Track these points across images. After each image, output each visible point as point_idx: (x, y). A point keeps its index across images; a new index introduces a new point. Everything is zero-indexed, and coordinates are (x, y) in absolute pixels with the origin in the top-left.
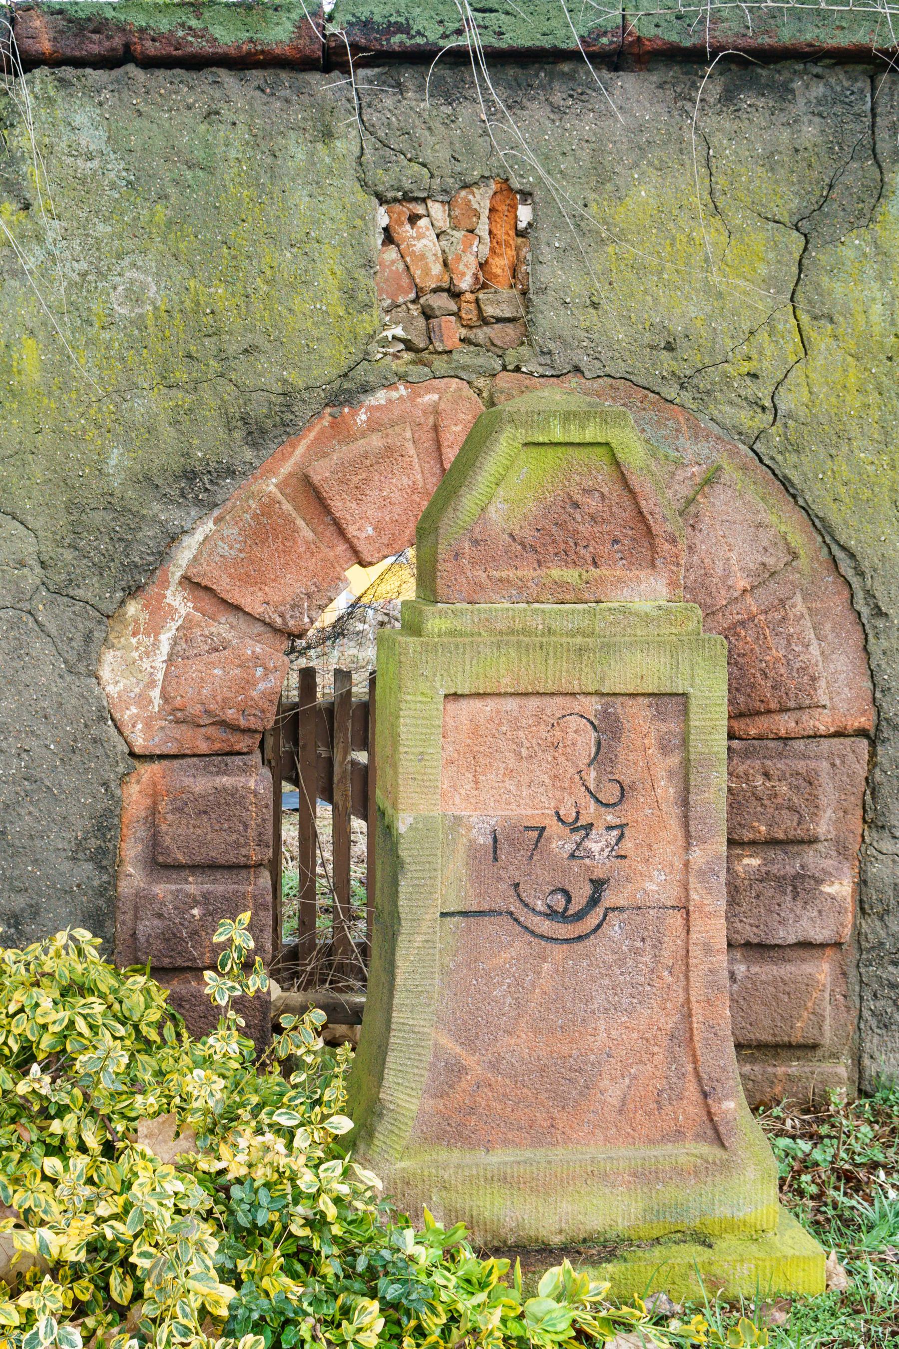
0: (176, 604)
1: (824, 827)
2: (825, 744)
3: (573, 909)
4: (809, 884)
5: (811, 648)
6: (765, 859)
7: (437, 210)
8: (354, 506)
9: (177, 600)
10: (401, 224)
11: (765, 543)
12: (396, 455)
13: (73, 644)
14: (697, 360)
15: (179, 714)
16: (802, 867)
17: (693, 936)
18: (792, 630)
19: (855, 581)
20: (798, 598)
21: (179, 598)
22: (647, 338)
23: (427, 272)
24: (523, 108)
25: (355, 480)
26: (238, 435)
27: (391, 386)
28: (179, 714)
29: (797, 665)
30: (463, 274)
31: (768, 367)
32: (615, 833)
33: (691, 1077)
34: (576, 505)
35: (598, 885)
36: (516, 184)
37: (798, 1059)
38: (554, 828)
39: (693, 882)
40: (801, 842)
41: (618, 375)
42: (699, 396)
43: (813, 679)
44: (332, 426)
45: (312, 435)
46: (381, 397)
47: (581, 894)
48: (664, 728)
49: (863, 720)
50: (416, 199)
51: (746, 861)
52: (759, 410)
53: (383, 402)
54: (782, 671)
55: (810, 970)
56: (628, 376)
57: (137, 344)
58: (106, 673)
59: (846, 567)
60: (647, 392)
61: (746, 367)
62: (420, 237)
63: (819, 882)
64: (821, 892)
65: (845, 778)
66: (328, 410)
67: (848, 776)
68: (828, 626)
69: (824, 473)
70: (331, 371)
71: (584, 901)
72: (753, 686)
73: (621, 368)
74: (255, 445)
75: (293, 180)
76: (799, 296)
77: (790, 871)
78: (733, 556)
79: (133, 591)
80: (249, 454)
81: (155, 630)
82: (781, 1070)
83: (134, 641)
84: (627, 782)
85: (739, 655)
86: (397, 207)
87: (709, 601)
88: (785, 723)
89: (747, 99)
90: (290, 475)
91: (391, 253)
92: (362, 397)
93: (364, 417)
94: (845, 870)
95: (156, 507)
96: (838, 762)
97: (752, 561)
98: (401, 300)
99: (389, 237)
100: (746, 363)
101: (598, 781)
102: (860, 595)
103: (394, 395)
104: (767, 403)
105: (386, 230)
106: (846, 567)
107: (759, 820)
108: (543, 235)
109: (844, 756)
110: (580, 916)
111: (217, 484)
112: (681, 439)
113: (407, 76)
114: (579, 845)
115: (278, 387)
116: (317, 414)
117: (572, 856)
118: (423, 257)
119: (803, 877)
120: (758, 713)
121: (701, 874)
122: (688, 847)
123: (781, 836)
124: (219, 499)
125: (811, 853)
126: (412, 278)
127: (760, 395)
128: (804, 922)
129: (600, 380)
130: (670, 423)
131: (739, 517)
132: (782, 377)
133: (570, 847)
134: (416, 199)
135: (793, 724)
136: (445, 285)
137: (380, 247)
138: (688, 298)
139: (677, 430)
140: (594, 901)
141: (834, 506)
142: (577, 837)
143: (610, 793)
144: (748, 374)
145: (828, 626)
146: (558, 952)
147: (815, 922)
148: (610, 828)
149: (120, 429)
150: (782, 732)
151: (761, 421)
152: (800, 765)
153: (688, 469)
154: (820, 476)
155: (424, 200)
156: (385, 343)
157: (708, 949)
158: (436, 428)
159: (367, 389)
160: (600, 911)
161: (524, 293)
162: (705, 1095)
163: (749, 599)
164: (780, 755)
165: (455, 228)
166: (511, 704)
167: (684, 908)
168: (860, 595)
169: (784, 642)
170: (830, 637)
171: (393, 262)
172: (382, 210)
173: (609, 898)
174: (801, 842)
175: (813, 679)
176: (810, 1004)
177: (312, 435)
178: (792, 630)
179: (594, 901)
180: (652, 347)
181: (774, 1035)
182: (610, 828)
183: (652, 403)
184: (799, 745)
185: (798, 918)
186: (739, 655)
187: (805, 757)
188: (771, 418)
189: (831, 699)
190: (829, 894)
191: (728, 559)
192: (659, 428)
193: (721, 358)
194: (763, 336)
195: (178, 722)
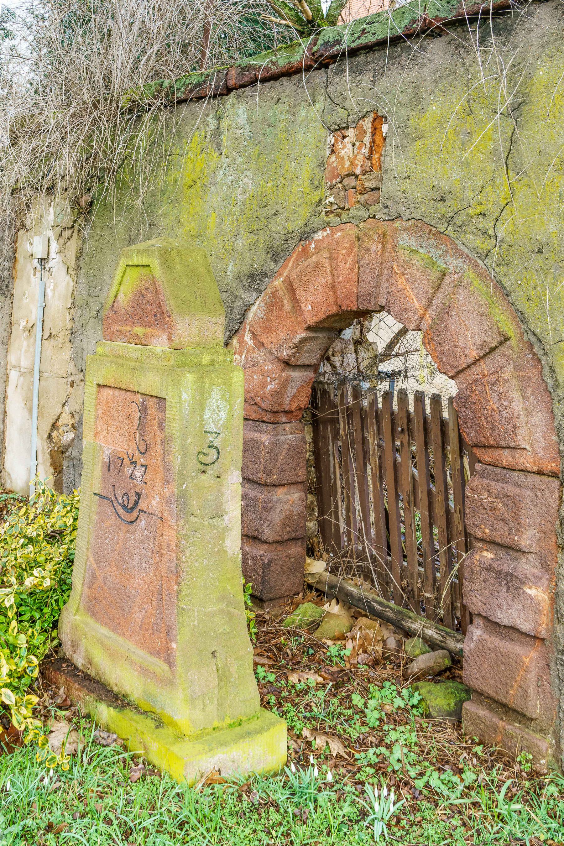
1: (527, 539)
2: (531, 479)
4: (516, 583)
5: (514, 404)
6: (496, 556)
8: (303, 293)
11: (486, 327)
12: (320, 266)
14: (455, 206)
18: (502, 390)
20: (511, 367)
22: (432, 194)
25: (305, 279)
26: (269, 256)
27: (324, 229)
29: (505, 415)
30: (357, 165)
31: (492, 210)
32: (143, 469)
34: (143, 295)
37: (520, 723)
41: (417, 218)
42: (457, 229)
43: (515, 427)
45: (295, 255)
46: (319, 235)
49: (553, 464)
51: (485, 553)
52: (488, 237)
53: (321, 237)
54: (496, 418)
55: (519, 652)
56: (422, 218)
57: (242, 213)
60: (431, 227)
61: (478, 210)
63: (523, 583)
64: (524, 592)
65: (543, 508)
67: (546, 506)
68: (530, 390)
69: (521, 280)
70: (300, 222)
72: (479, 425)
73: (417, 214)
74: (275, 261)
75: (299, 126)
76: (509, 161)
77: (505, 568)
78: (469, 334)
80: (272, 265)
82: (501, 724)
85: (471, 402)
87: (455, 364)
88: (506, 457)
92: (313, 235)
93: (313, 246)
94: (544, 580)
95: (241, 291)
96: (539, 494)
97: (479, 338)
100: (479, 207)
103: (325, 233)
104: (491, 233)
106: (537, 348)
107: (484, 524)
109: (543, 490)
111: (262, 280)
112: (448, 257)
115: (283, 232)
119: (512, 575)
120: (491, 447)
124: (262, 288)
125: (525, 560)
127: (487, 227)
128: (512, 611)
129: (410, 222)
130: (443, 247)
131: (471, 308)
132: (498, 215)
135: (511, 459)
138: (451, 168)
139: (446, 251)
140: (136, 503)
141: (527, 304)
144: (481, 214)
145: (530, 390)
147: (520, 614)
149: (233, 254)
151: (488, 245)
152: (510, 489)
153: (452, 276)
154: (519, 282)
159: (315, 231)
164: (503, 480)
166: (117, 393)
169: (497, 398)
170: (532, 398)
173: (142, 505)
175: (515, 427)
176: (518, 679)
177: (295, 255)
178: (502, 390)
180: (435, 200)
181: (497, 694)
183: (434, 235)
184: (515, 475)
185: (509, 607)
186: (471, 402)
187: (517, 485)
188: (494, 242)
189: (532, 445)
190: (528, 594)
191: (466, 337)
192: (437, 250)
193: (466, 204)
194: (488, 189)
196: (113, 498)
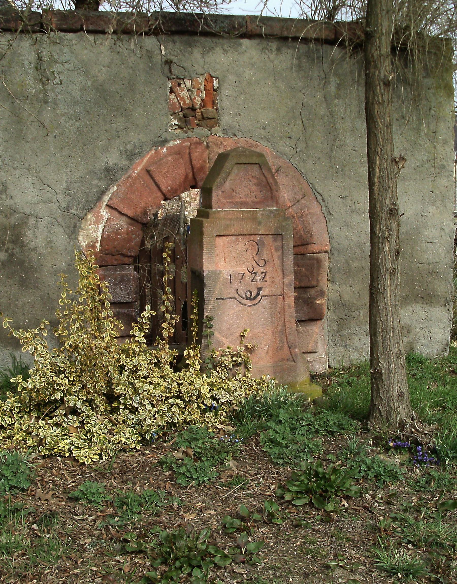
0: (104, 214)
3: (252, 296)
7: (188, 83)
9: (104, 213)
10: (175, 86)
13: (70, 228)
15: (107, 252)
16: (310, 295)
17: (286, 303)
19: (322, 203)
21: (105, 212)
23: (185, 102)
24: (214, 50)
27: (175, 140)
28: (107, 252)
33: (286, 343)
35: (259, 289)
36: (213, 74)
38: (247, 273)
39: (285, 288)
40: (309, 287)
44: (155, 153)
47: (254, 293)
48: (276, 244)
50: (180, 78)
58: (81, 238)
59: (319, 198)
62: (182, 91)
66: (154, 148)
71: (255, 294)
79: (90, 210)
81: (97, 222)
83: (90, 227)
84: (266, 260)
86: (174, 81)
89: (284, 50)
90: (142, 170)
91: (173, 96)
98: (176, 111)
99: (172, 91)
101: (259, 260)
102: (324, 208)
104: (294, 147)
105: (171, 88)
106: (319, 198)
108: (223, 92)
110: (255, 298)
113: (176, 38)
114: (254, 278)
116: (151, 150)
117: (252, 281)
118: (183, 98)
121: (287, 285)
122: (283, 278)
123: (303, 285)
126: (180, 104)
133: (251, 279)
134: (180, 78)
136: (191, 107)
137: (169, 94)
140: (258, 294)
142: (253, 276)
143: (262, 263)
146: (249, 309)
148: (262, 273)
150: (303, 252)
155: (183, 79)
156: (171, 126)
157: (289, 306)
158: (190, 154)
160: (260, 297)
161: (217, 110)
162: (290, 348)
163: (290, 209)
165: (194, 88)
167: (283, 295)
168: (324, 208)
171: (173, 99)
172: (169, 82)
174: (309, 287)
179: (258, 294)
182: (262, 273)
195: (106, 254)
196: (236, 296)
